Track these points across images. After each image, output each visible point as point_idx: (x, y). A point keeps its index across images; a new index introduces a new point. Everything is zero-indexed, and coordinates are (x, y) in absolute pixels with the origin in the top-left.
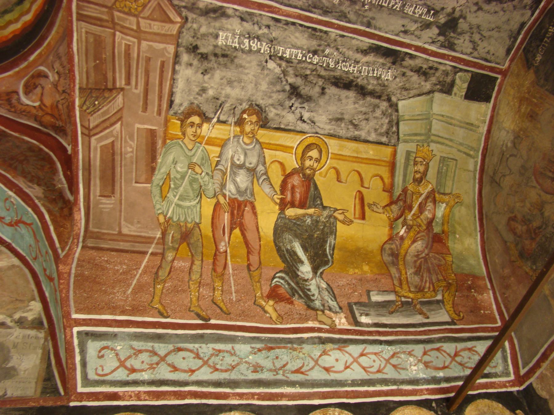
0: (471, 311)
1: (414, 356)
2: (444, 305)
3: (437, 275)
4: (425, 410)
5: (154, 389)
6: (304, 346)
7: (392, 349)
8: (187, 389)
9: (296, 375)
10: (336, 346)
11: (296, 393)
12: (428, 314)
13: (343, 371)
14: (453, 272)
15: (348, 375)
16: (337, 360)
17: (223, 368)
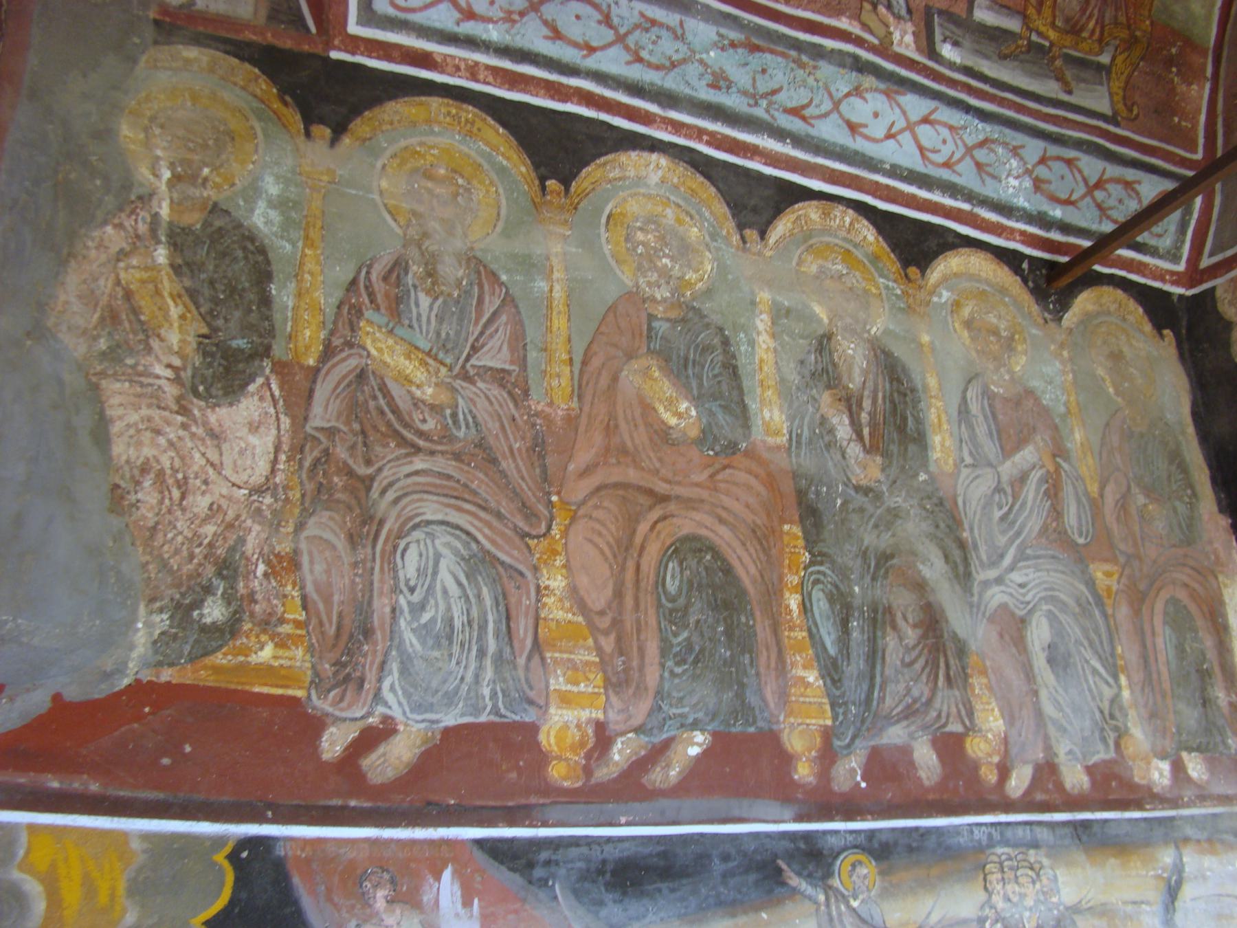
0: (1156, 111)
1: (1022, 159)
2: (1109, 79)
3: (1116, 10)
4: (1006, 269)
5: (507, 64)
6: (821, 63)
7: (984, 130)
8: (574, 82)
9: (791, 118)
10: (882, 86)
11: (782, 154)
12: (1073, 84)
13: (882, 141)
14: (1150, 15)
15: (888, 152)
16: (876, 115)
17: (653, 60)
